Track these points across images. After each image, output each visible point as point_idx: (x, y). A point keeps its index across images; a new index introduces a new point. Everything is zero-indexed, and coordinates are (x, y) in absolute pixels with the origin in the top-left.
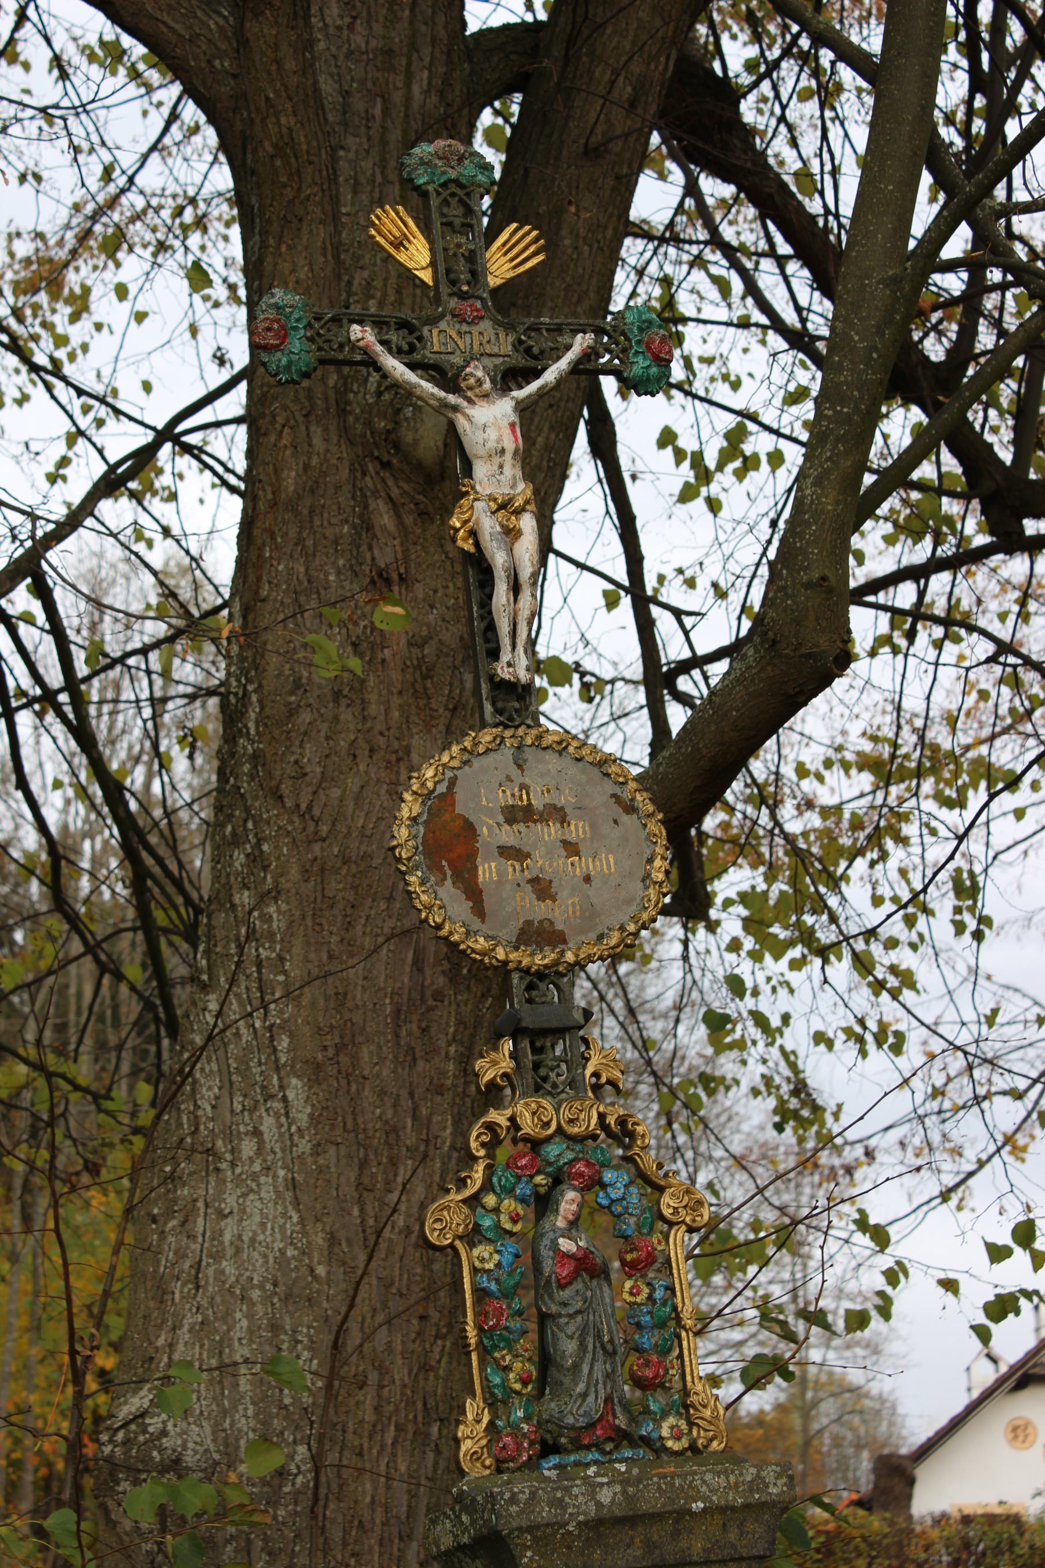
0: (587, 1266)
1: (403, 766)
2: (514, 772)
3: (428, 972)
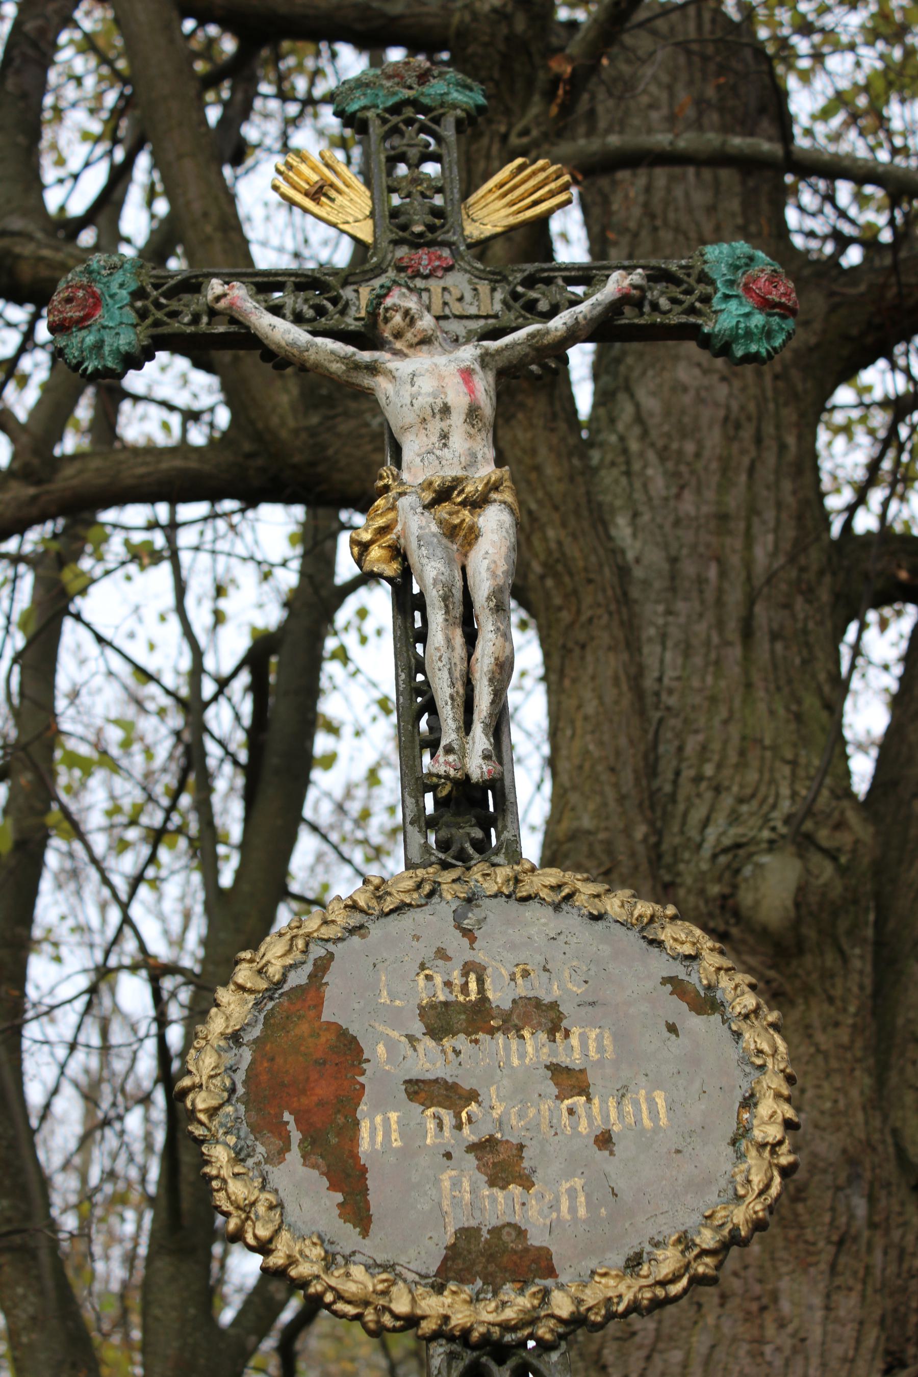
1: (769, 1318)
2: (455, 943)
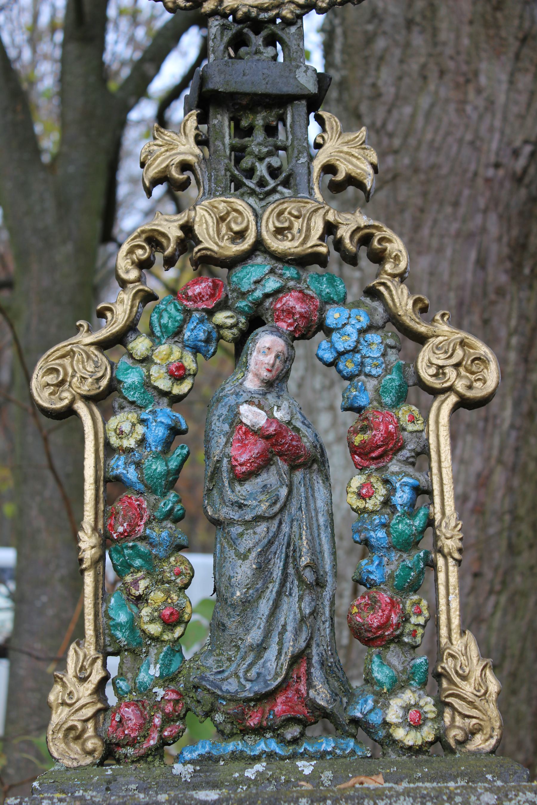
0: (287, 452)
3: (491, 270)
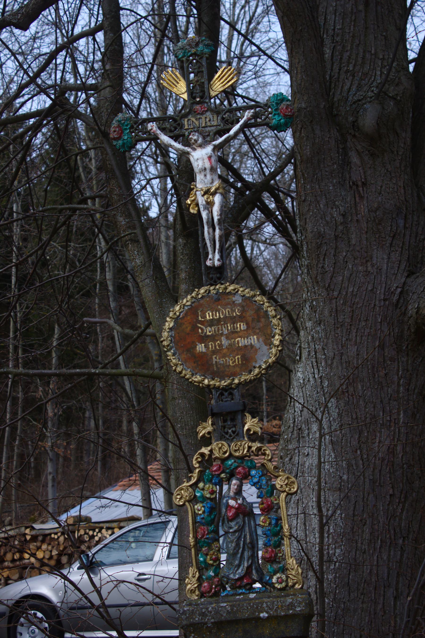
1: (369, 264)
